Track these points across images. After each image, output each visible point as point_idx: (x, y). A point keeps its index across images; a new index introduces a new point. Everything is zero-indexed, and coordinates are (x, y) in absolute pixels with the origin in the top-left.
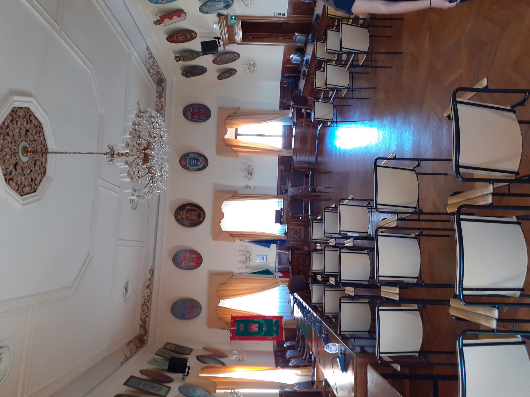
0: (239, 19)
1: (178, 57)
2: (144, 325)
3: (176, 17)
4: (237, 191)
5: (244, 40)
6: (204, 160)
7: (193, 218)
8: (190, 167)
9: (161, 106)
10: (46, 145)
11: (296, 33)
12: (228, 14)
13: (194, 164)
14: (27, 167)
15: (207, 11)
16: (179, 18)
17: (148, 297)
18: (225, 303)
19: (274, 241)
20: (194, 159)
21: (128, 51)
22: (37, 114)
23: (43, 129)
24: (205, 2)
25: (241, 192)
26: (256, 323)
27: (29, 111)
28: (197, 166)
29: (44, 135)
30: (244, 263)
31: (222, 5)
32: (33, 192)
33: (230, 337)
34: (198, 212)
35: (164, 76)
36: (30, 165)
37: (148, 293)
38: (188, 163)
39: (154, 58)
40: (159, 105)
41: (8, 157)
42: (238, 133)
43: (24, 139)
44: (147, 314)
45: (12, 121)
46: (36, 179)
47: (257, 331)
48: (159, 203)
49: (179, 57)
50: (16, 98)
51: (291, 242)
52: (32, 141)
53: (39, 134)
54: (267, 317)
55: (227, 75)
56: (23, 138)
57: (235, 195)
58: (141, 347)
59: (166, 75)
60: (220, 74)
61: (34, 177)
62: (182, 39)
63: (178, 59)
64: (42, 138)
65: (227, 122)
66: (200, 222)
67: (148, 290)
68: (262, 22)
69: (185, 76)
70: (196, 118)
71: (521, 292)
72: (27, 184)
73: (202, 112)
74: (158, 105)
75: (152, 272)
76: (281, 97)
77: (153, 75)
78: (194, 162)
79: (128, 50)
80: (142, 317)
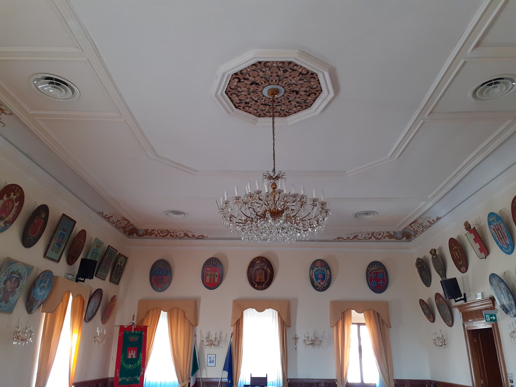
2: (148, 233)
3: (479, 247)
4: (290, 327)
5: (469, 331)
6: (324, 287)
7: (257, 276)
8: (314, 270)
9: (380, 237)
10: (289, 115)
12: (497, 310)
13: (318, 276)
14: (258, 96)
16: (478, 252)
17: (176, 235)
18: (163, 319)
19: (231, 376)
20: (324, 276)
21: (430, 197)
22: (318, 101)
23: (305, 109)
25: (289, 331)
26: (137, 355)
27: (319, 92)
28: (316, 279)
31: (506, 302)
32: (235, 105)
33: (124, 326)
34: (264, 282)
35: (413, 239)
36: (262, 99)
37: (180, 235)
38: (318, 268)
39: (430, 226)
40: (380, 235)
41: (261, 74)
42: (361, 326)
43: (287, 90)
44: (158, 236)
45: (301, 73)
46: (250, 107)
47: (128, 357)
50: (327, 74)
52: (288, 99)
53: (298, 106)
54: (143, 369)
55: (427, 312)
56: (288, 89)
58: (125, 232)
59: (415, 241)
61: (251, 105)
62: (456, 256)
63: (433, 253)
64: (295, 109)
65: (372, 313)
66: (253, 285)
67: (182, 235)
70: (372, 276)
72: (240, 98)
75: (201, 237)
79: (430, 197)
80: (156, 231)
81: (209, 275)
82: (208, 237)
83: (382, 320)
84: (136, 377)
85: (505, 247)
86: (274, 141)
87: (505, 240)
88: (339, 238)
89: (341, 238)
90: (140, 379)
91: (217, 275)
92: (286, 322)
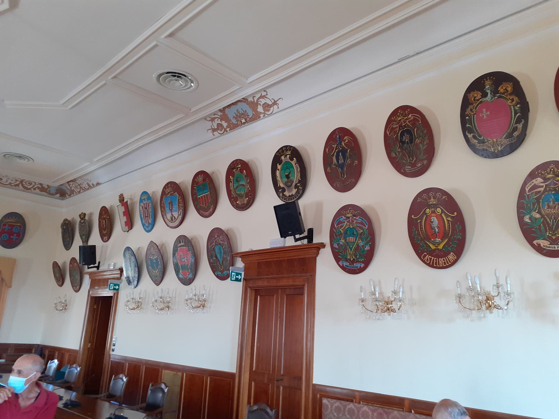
0: (115, 293)
1: (85, 217)
5: (92, 298)
9: (29, 187)
11: (80, 368)
21: (95, 160)
24: (136, 256)
39: (88, 189)
49: (85, 218)
55: (57, 275)
60: (59, 266)
63: (82, 217)
68: (108, 324)
69: (63, 222)
73: (12, 237)
74: (31, 184)
77: (69, 185)
85: (147, 225)
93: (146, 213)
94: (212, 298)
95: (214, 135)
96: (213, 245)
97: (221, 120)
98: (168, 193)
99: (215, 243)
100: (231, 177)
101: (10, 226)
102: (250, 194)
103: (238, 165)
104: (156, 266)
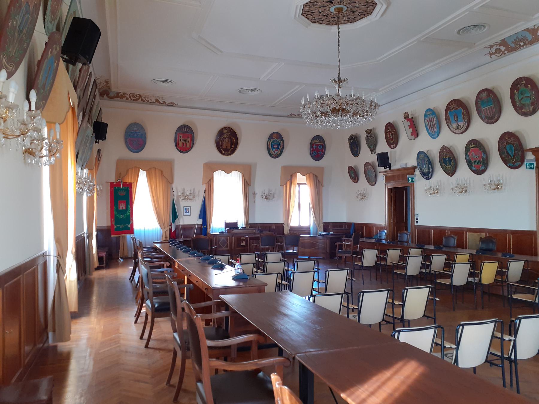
2: (119, 96)
6: (277, 155)
8: (271, 141)
12: (416, 175)
13: (274, 146)
15: (420, 157)
16: (410, 134)
18: (143, 176)
20: (278, 146)
25: (250, 188)
26: (127, 207)
29: (344, 23)
30: (183, 193)
37: (151, 100)
38: (274, 140)
44: (130, 99)
47: (119, 209)
48: (237, 112)
49: (371, 132)
50: (385, 6)
51: (215, 238)
54: (132, 219)
55: (353, 175)
57: (247, 184)
64: (359, 17)
65: (312, 175)
66: (220, 151)
67: (154, 100)
71: (506, 334)
75: (172, 104)
76: (333, 223)
78: (275, 146)
80: (127, 94)
81: (181, 140)
82: (178, 105)
83: (318, 180)
84: (127, 225)
85: (433, 133)
86: (339, 43)
87: (434, 128)
88: (291, 115)
89: (294, 114)
90: (131, 226)
91: (188, 141)
92: (248, 181)
93: (432, 125)
94: (506, 182)
95: (491, 58)
96: (504, 145)
97: (499, 46)
98: (453, 108)
99: (506, 143)
100: (515, 91)
101: (316, 145)
102: (536, 103)
103: (523, 81)
104: (449, 163)
